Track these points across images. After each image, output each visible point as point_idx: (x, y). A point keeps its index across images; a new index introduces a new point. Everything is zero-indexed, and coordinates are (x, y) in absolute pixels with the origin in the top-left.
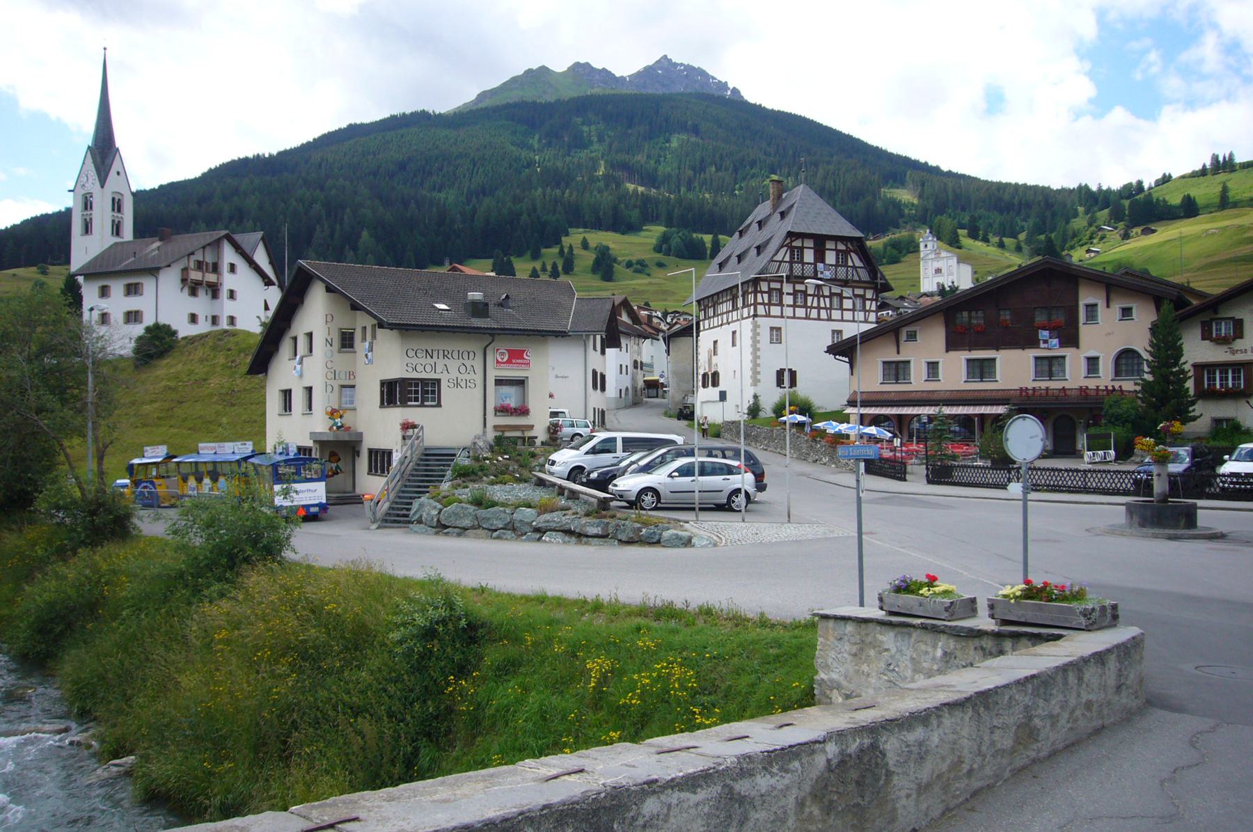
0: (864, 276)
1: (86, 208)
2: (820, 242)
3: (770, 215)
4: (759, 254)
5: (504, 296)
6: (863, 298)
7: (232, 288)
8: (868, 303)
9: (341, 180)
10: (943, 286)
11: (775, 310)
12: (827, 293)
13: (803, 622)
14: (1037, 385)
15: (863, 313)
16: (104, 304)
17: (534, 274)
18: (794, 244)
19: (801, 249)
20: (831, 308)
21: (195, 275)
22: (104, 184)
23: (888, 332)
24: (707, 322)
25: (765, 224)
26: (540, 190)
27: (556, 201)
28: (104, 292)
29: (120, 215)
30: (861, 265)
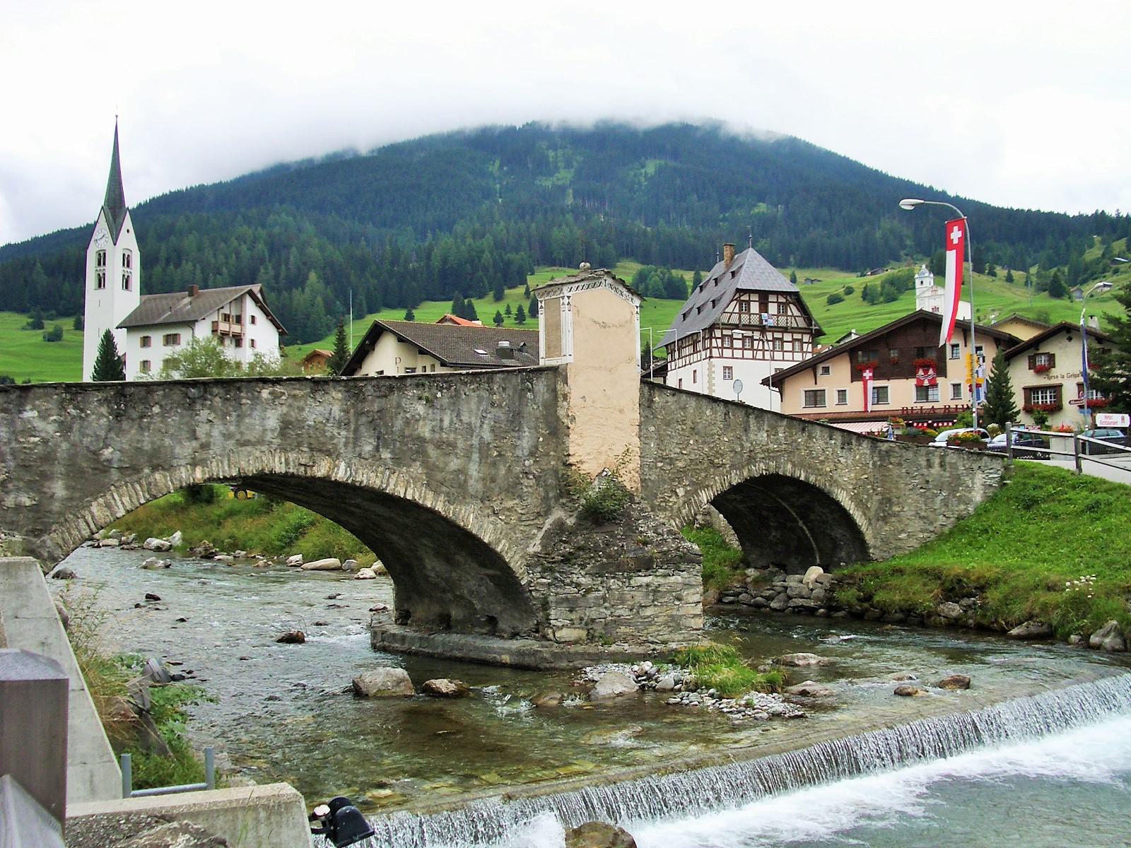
0: (802, 323)
1: (99, 264)
2: (764, 296)
3: (724, 273)
4: (714, 307)
5: (522, 344)
6: (781, 340)
8: (805, 345)
9: (283, 215)
11: (727, 353)
12: (770, 338)
14: (919, 406)
16: (146, 354)
17: (498, 319)
18: (742, 298)
19: (748, 302)
20: (773, 351)
21: (223, 327)
22: (117, 240)
23: (809, 367)
24: (673, 363)
25: (720, 281)
26: (502, 223)
27: (520, 236)
28: (146, 342)
29: (129, 270)
30: (799, 314)
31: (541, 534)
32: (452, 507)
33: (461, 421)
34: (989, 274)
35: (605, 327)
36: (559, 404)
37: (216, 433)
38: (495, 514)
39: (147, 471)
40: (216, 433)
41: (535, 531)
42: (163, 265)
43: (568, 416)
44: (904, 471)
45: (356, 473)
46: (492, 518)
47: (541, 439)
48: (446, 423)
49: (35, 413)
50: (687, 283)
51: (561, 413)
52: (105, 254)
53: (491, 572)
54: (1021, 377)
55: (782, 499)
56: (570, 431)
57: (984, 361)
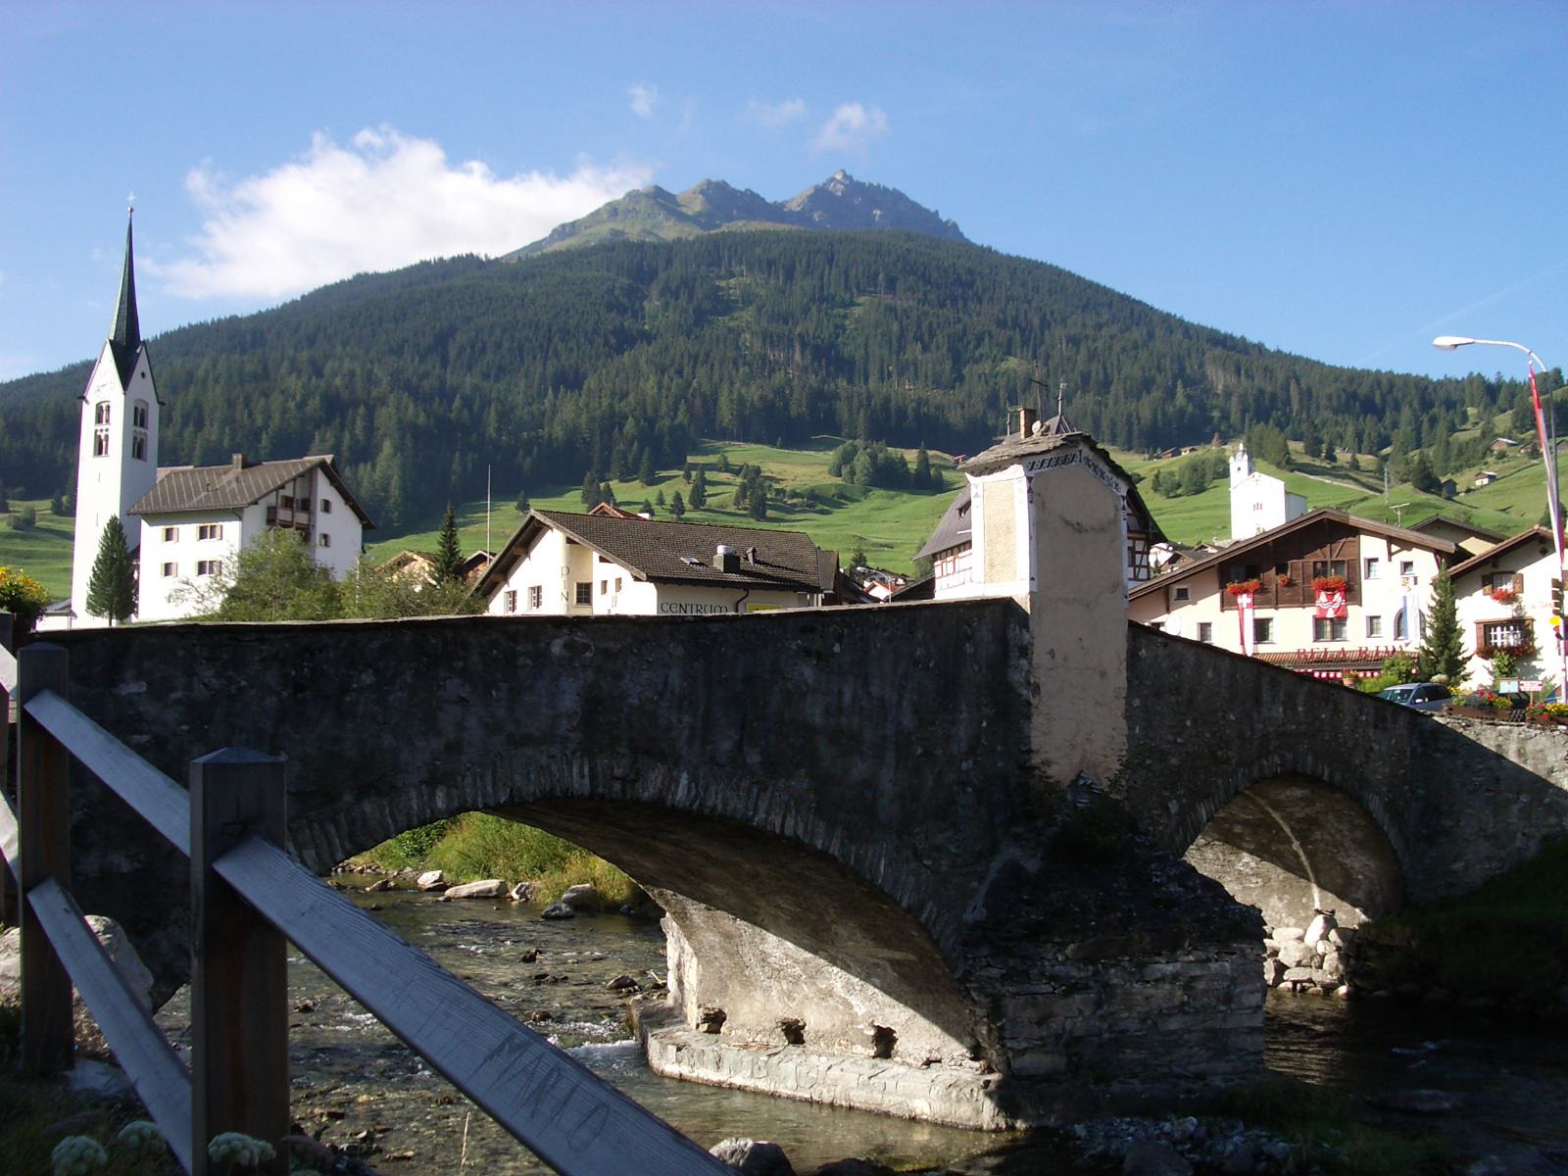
7: (325, 532)
10: (62, 410)
13: (1036, 760)
15: (1132, 569)
29: (143, 430)
31: (984, 890)
32: (854, 848)
33: (869, 693)
34: (1326, 458)
35: (1080, 532)
36: (1012, 662)
37: (472, 722)
38: (918, 856)
39: (348, 798)
40: (472, 722)
41: (975, 884)
42: (178, 427)
43: (1029, 683)
44: (1460, 762)
45: (705, 792)
46: (913, 865)
47: (984, 724)
48: (847, 697)
49: (141, 687)
50: (909, 466)
51: (1016, 677)
52: (108, 407)
53: (898, 955)
54: (1475, 608)
55: (1273, 808)
56: (1033, 710)
57: (1416, 583)
